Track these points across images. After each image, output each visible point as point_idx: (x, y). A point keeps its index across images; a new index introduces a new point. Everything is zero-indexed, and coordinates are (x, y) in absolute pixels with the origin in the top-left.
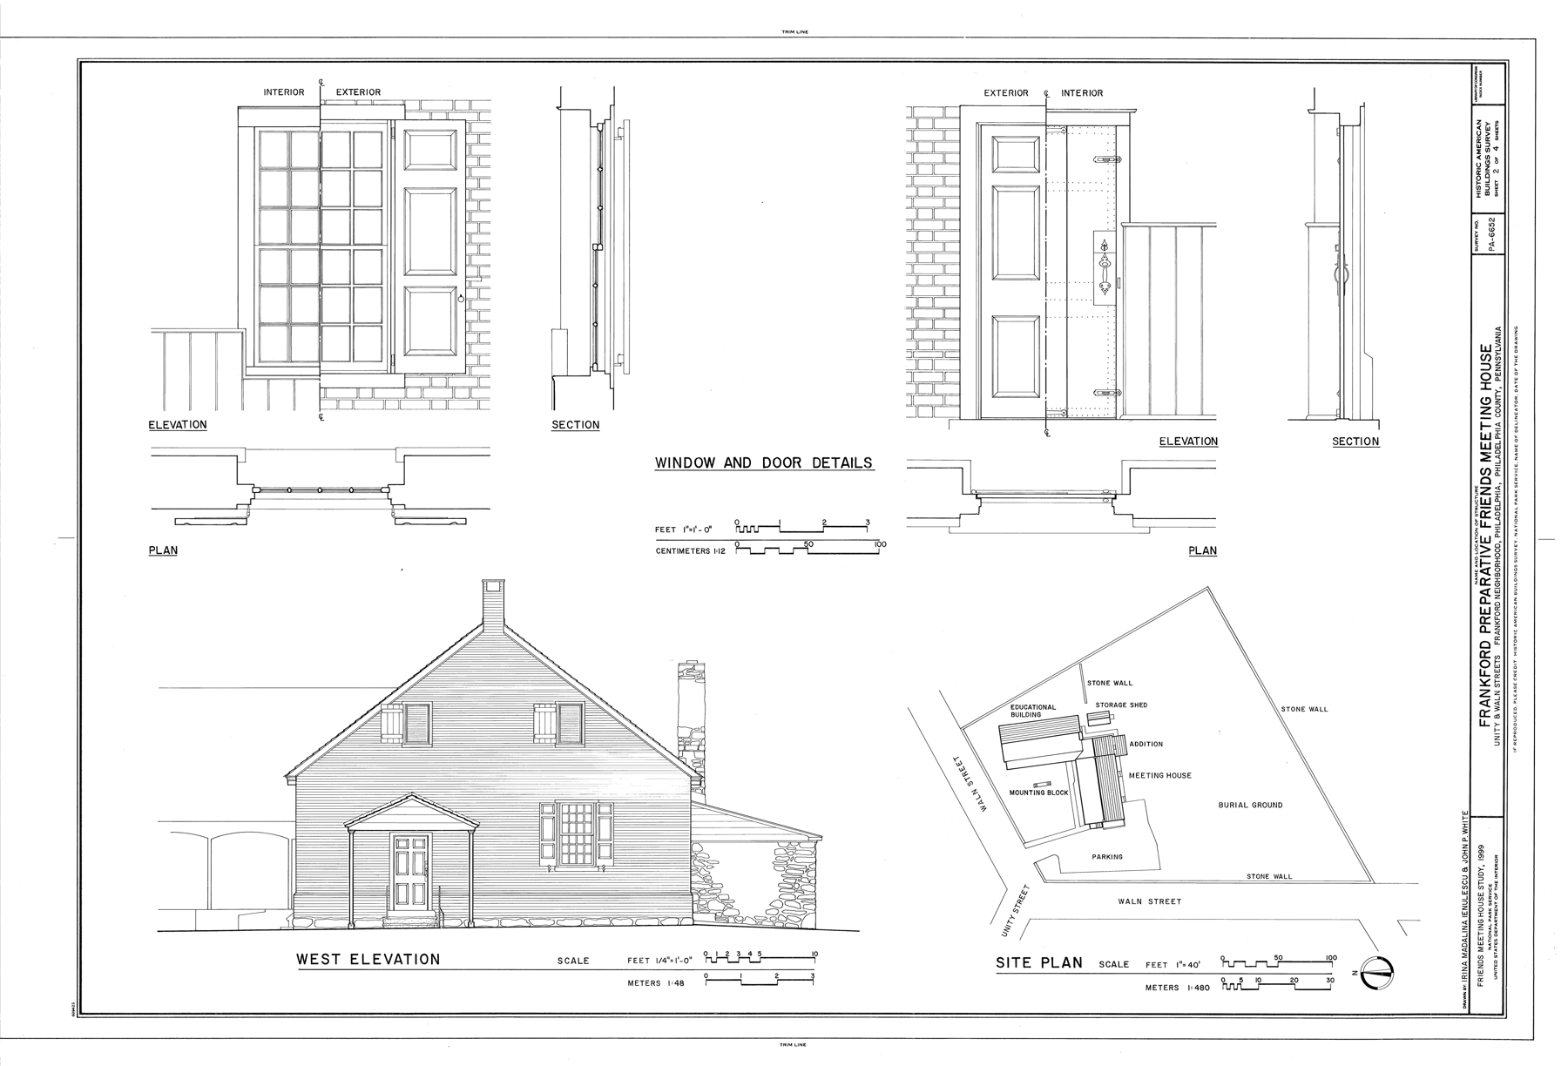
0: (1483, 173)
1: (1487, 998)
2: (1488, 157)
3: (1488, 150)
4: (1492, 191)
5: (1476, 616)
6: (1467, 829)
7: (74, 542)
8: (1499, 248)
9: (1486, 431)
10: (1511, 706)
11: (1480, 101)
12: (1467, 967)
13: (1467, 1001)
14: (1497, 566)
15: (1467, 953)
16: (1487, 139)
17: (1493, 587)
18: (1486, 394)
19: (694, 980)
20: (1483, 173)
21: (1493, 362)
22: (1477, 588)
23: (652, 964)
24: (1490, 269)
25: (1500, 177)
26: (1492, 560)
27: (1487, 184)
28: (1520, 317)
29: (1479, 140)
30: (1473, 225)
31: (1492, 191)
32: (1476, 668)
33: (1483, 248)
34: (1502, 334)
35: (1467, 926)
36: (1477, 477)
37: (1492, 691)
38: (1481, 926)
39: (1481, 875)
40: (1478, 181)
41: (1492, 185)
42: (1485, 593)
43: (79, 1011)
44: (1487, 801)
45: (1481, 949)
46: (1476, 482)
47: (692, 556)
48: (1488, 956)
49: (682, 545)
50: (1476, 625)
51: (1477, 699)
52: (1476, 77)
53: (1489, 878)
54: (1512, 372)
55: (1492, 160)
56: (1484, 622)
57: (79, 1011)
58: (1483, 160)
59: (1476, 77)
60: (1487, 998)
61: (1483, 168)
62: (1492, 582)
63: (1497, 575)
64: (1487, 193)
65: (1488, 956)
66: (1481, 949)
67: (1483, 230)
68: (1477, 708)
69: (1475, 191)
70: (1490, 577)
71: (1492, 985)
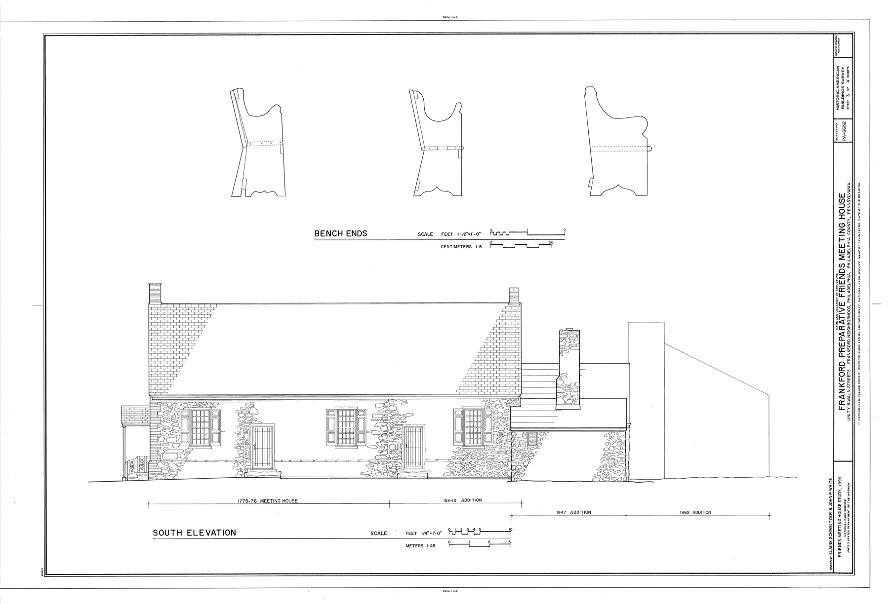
0: (840, 96)
3: (843, 83)
4: (845, 106)
5: (837, 347)
8: (849, 138)
9: (842, 243)
10: (857, 398)
12: (832, 544)
13: (832, 566)
14: (848, 318)
16: (843, 77)
17: (846, 331)
18: (842, 221)
19: (441, 544)
20: (840, 96)
21: (846, 203)
23: (419, 535)
24: (844, 150)
25: (850, 99)
26: (846, 315)
27: (843, 102)
28: (861, 177)
29: (838, 77)
30: (835, 126)
31: (845, 106)
32: (837, 377)
33: (840, 139)
34: (852, 187)
36: (837, 269)
37: (846, 393)
38: (840, 523)
39: (840, 494)
40: (838, 101)
41: (845, 103)
42: (842, 334)
43: (45, 573)
44: (844, 453)
45: (840, 536)
46: (837, 272)
48: (844, 540)
50: (837, 352)
51: (837, 394)
52: (836, 42)
55: (845, 89)
56: (841, 351)
57: (45, 573)
58: (840, 88)
59: (836, 42)
61: (840, 93)
62: (846, 328)
63: (849, 325)
64: (843, 108)
66: (840, 536)
67: (840, 129)
68: (837, 399)
69: (836, 106)
70: (845, 324)
71: (846, 557)
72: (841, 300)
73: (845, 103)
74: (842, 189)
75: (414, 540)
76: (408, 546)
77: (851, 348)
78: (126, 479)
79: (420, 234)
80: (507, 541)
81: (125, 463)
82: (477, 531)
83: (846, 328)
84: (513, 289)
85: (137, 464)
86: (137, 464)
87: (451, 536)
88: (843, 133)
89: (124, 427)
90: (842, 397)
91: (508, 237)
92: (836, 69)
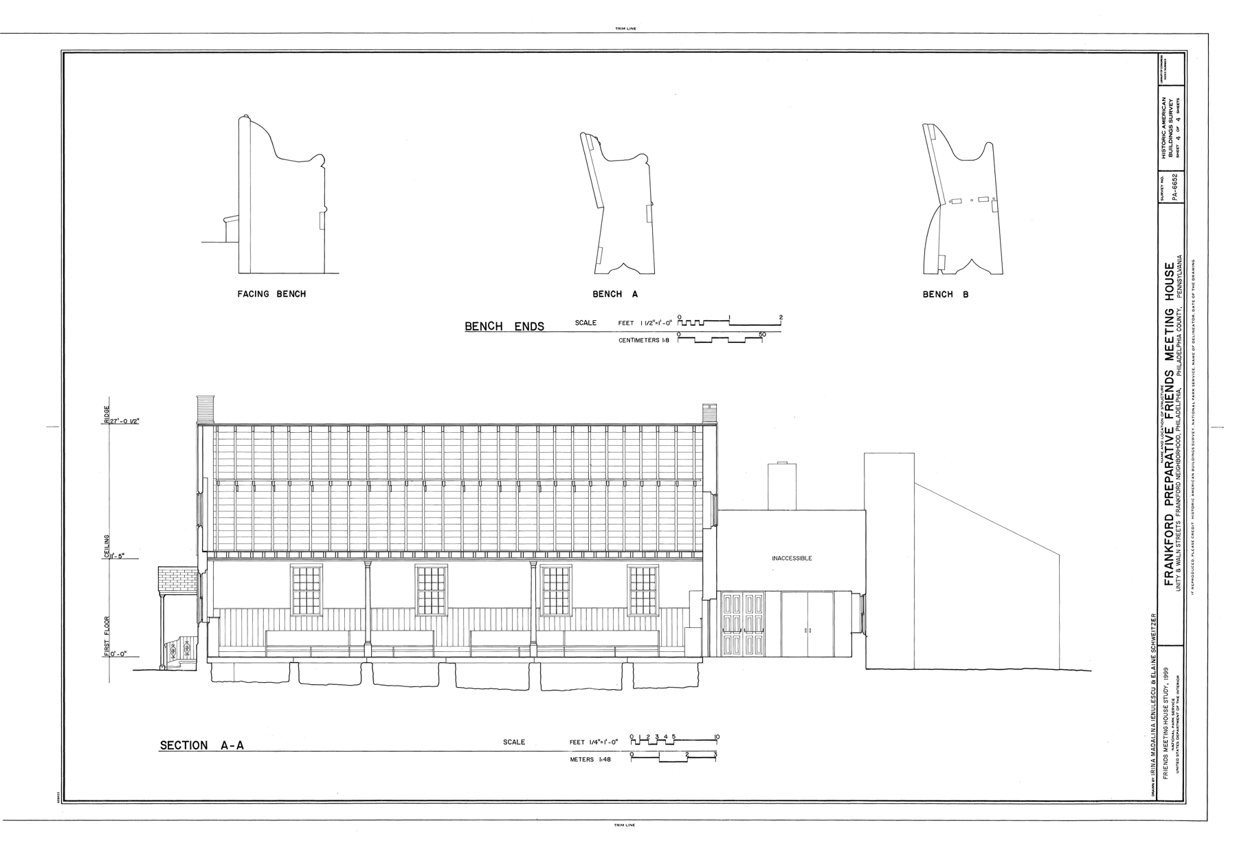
0: (1167, 139)
1: (1171, 788)
2: (1171, 127)
3: (1171, 121)
4: (1174, 153)
5: (1162, 492)
6: (1155, 660)
7: (59, 430)
8: (1180, 198)
9: (1169, 336)
10: (1190, 558)
11: (1165, 82)
12: (1155, 763)
13: (1155, 791)
14: (1178, 453)
15: (1155, 752)
16: (1171, 113)
18: (1169, 305)
20: (1167, 139)
22: (1162, 469)
24: (1172, 214)
27: (1171, 148)
28: (1196, 252)
29: (1164, 111)
30: (1160, 180)
31: (1174, 153)
32: (1162, 537)
33: (1168, 197)
35: (1155, 729)
36: (1162, 377)
37: (1173, 560)
38: (1166, 732)
39: (1166, 691)
40: (1163, 146)
41: (1174, 149)
42: (1169, 473)
43: (63, 798)
45: (1166, 750)
46: (1162, 382)
47: (645, 344)
48: (1172, 755)
49: (638, 336)
50: (1162, 499)
51: (1162, 562)
52: (1161, 64)
53: (1172, 694)
54: (1190, 296)
55: (1174, 129)
56: (1168, 496)
57: (63, 798)
58: (1167, 129)
59: (1161, 64)
60: (1171, 788)
61: (1167, 135)
62: (1174, 465)
63: (1178, 461)
64: (1171, 155)
65: (1172, 755)
66: (1166, 750)
68: (1163, 570)
69: (1161, 152)
70: (1173, 459)
71: (1175, 778)
72: (1169, 424)
73: (1174, 149)
74: (1170, 255)
75: (582, 753)
76: (574, 759)
77: (1181, 494)
78: (164, 668)
79: (578, 323)
80: (712, 754)
81: (164, 645)
82: (670, 740)
83: (1174, 465)
84: (710, 408)
85: (180, 648)
86: (180, 648)
87: (633, 747)
88: (1173, 190)
89: (162, 596)
90: (1169, 566)
91: (701, 328)
92: (1161, 102)
